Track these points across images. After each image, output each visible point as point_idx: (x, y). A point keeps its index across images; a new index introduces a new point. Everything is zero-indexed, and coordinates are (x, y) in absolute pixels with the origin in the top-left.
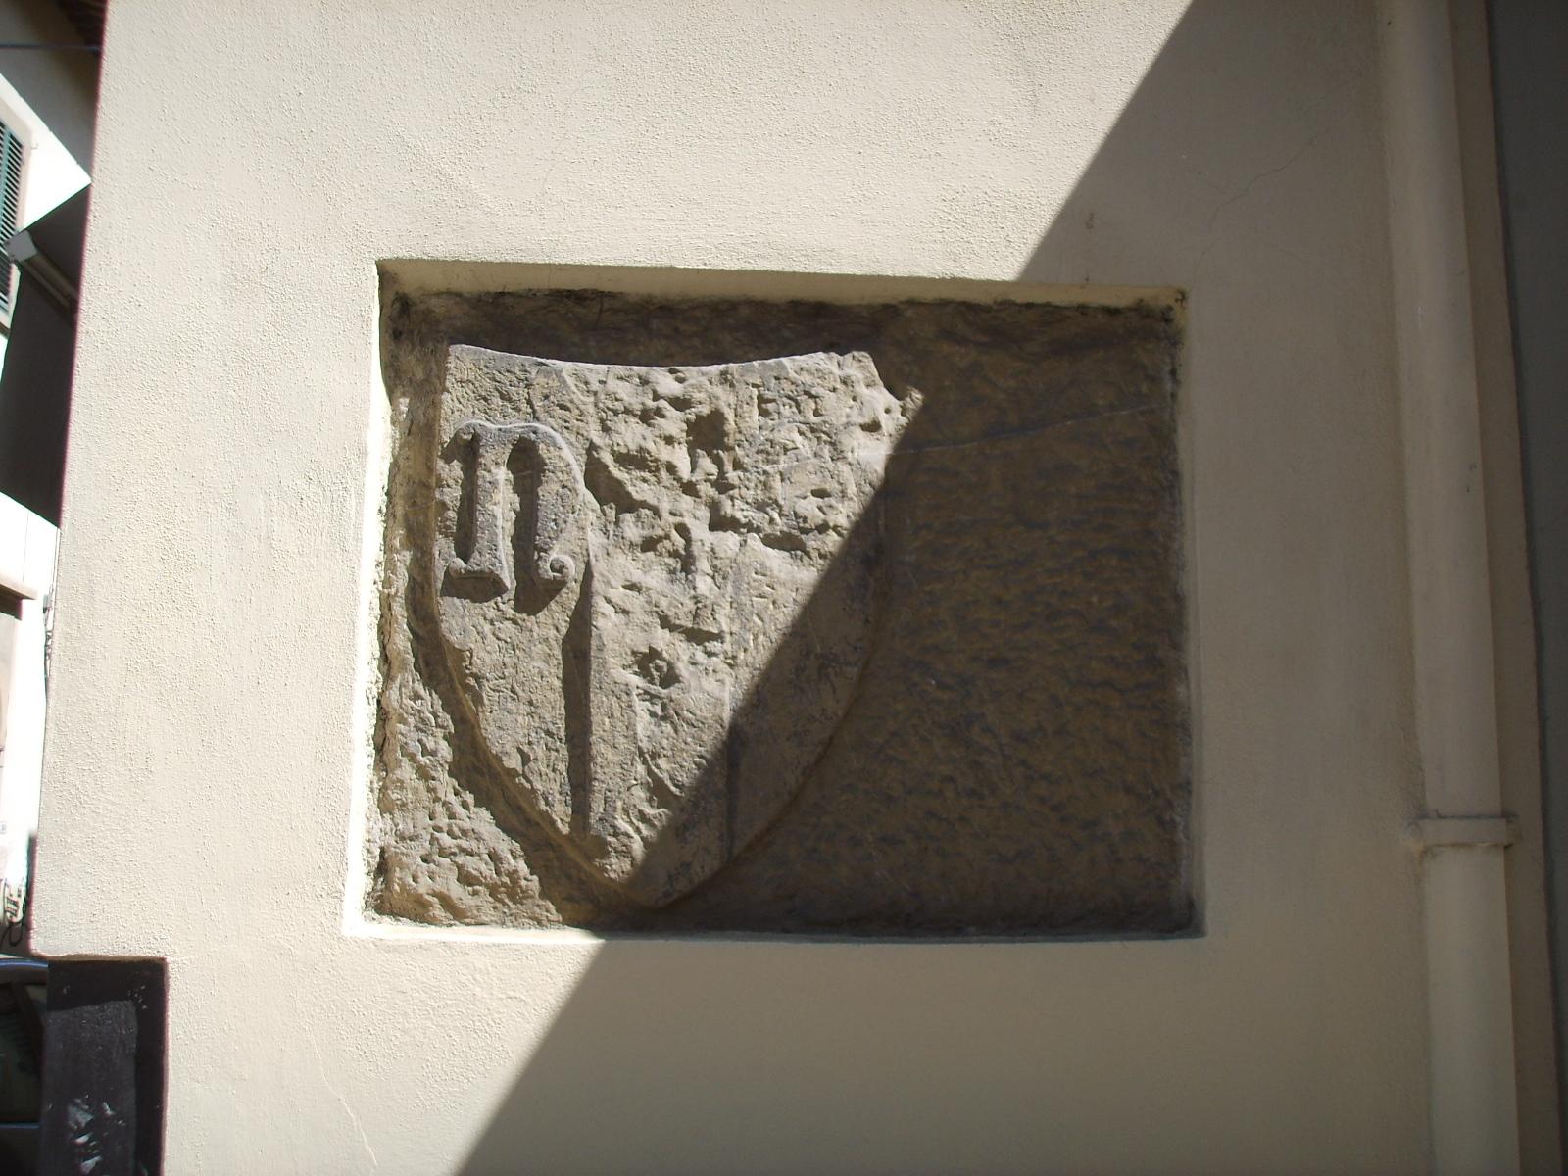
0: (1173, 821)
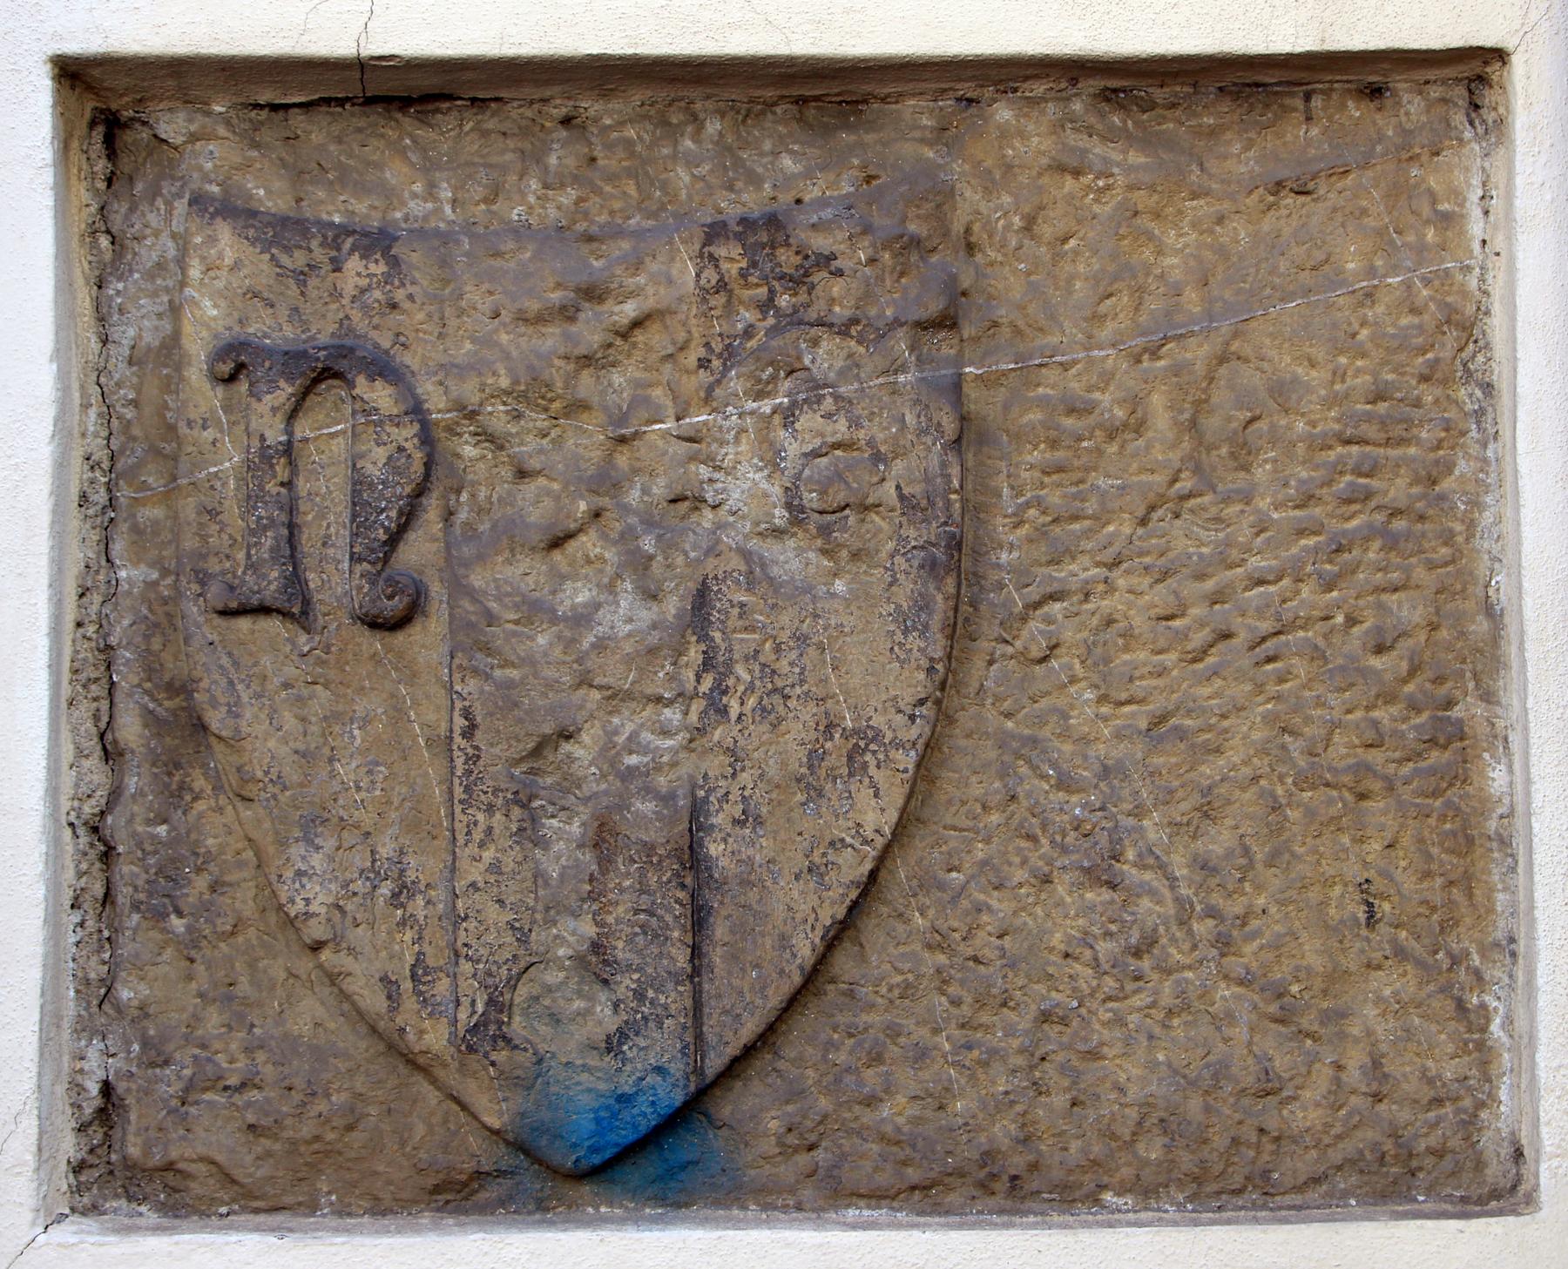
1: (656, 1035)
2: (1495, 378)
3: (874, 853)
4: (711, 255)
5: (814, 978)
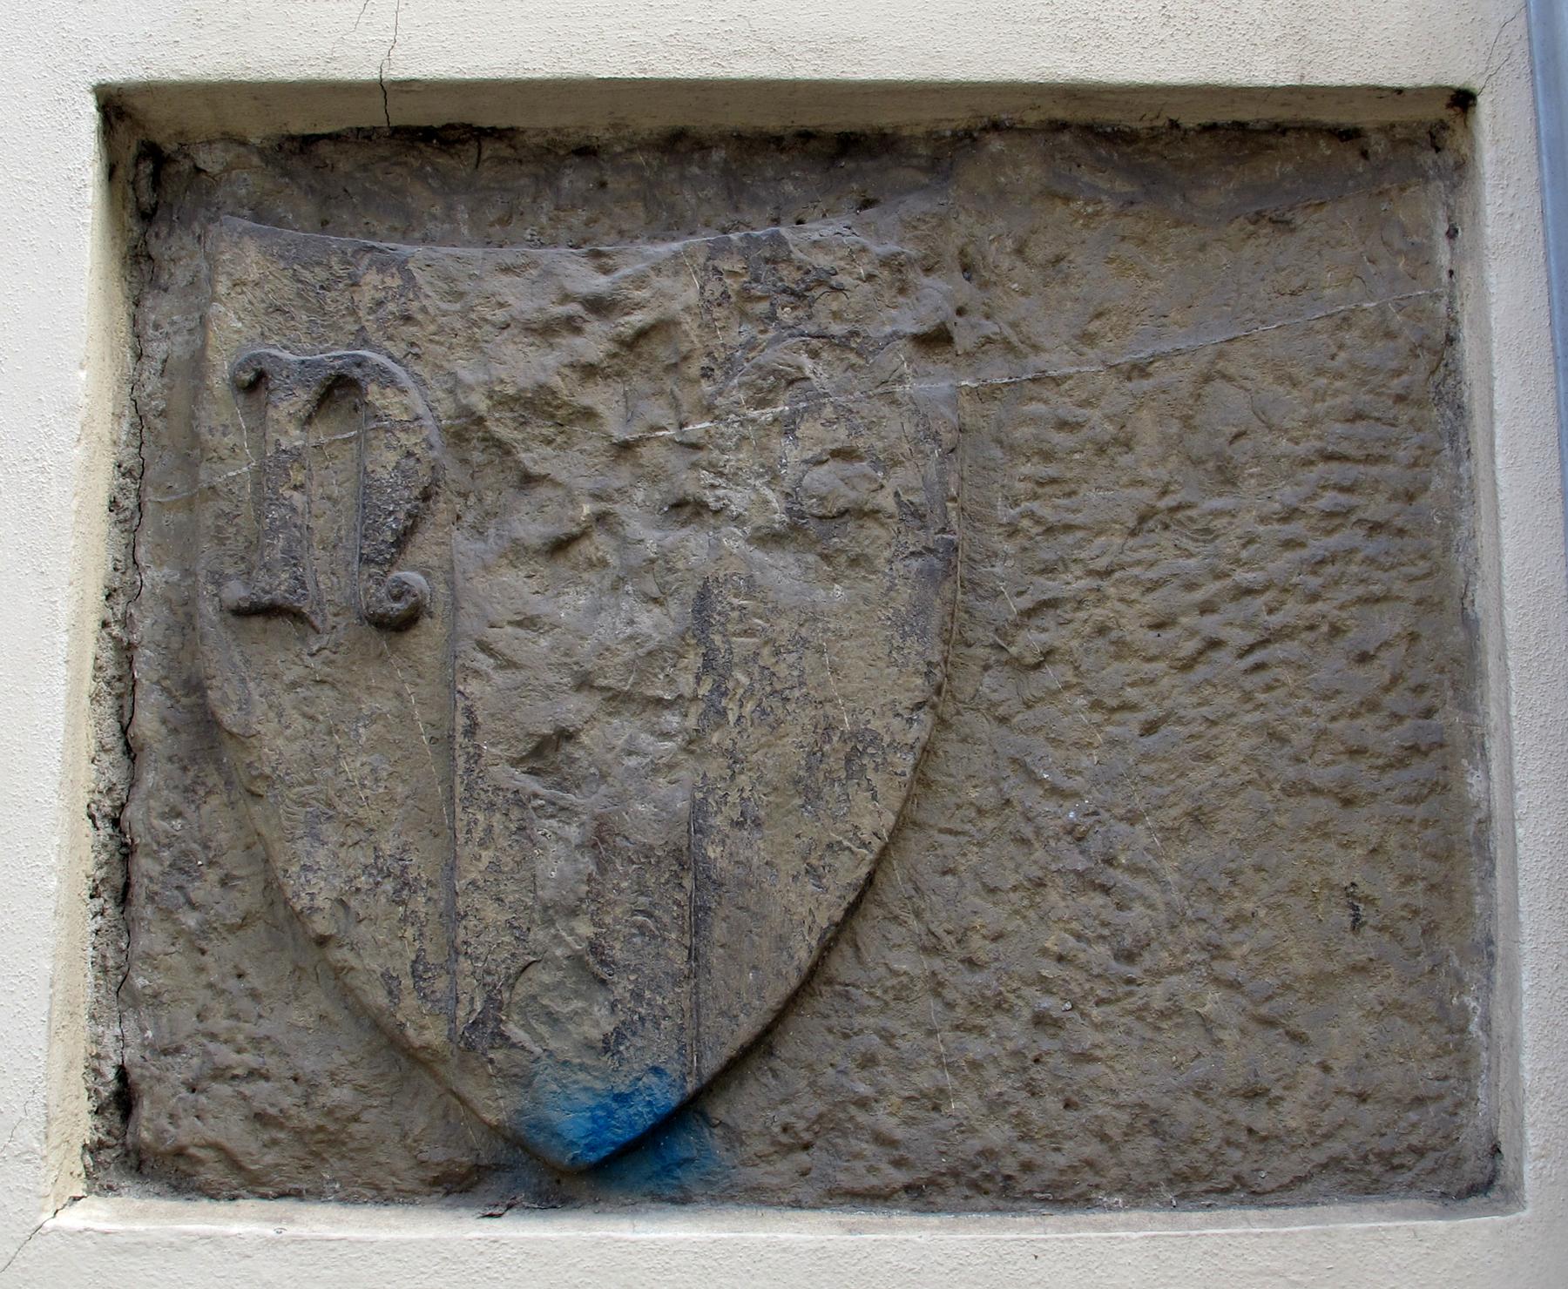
0: (1463, 1008)
1: (654, 1035)
2: (1465, 399)
3: (871, 857)
4: (715, 269)
5: (813, 978)
